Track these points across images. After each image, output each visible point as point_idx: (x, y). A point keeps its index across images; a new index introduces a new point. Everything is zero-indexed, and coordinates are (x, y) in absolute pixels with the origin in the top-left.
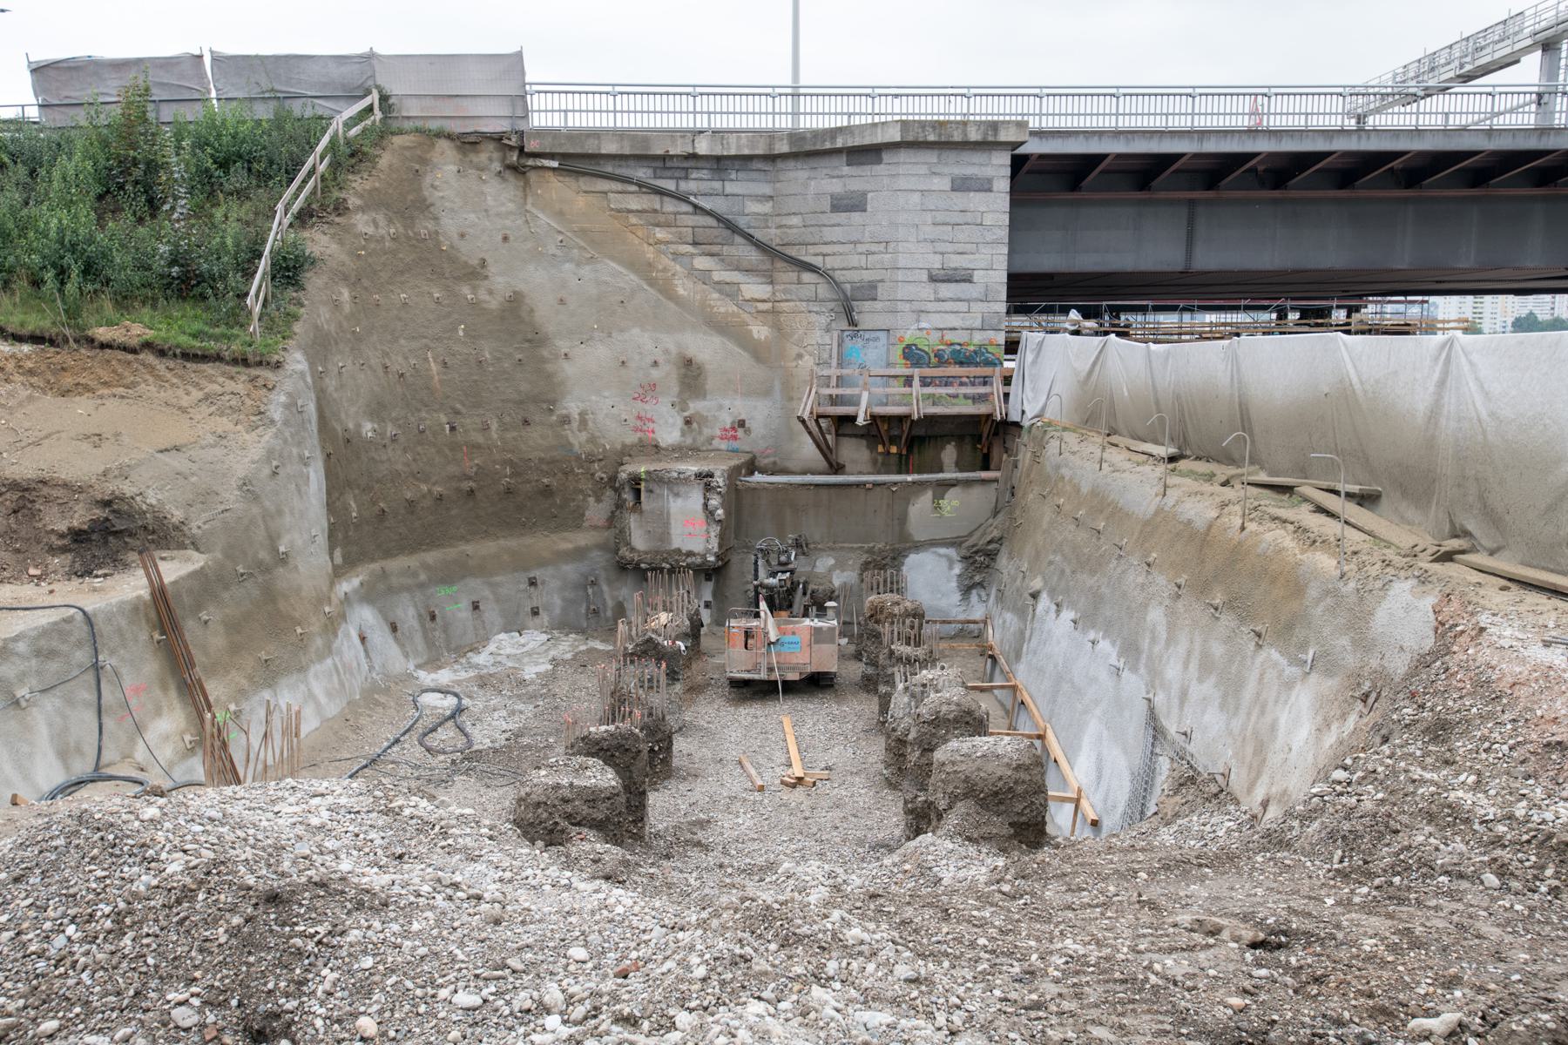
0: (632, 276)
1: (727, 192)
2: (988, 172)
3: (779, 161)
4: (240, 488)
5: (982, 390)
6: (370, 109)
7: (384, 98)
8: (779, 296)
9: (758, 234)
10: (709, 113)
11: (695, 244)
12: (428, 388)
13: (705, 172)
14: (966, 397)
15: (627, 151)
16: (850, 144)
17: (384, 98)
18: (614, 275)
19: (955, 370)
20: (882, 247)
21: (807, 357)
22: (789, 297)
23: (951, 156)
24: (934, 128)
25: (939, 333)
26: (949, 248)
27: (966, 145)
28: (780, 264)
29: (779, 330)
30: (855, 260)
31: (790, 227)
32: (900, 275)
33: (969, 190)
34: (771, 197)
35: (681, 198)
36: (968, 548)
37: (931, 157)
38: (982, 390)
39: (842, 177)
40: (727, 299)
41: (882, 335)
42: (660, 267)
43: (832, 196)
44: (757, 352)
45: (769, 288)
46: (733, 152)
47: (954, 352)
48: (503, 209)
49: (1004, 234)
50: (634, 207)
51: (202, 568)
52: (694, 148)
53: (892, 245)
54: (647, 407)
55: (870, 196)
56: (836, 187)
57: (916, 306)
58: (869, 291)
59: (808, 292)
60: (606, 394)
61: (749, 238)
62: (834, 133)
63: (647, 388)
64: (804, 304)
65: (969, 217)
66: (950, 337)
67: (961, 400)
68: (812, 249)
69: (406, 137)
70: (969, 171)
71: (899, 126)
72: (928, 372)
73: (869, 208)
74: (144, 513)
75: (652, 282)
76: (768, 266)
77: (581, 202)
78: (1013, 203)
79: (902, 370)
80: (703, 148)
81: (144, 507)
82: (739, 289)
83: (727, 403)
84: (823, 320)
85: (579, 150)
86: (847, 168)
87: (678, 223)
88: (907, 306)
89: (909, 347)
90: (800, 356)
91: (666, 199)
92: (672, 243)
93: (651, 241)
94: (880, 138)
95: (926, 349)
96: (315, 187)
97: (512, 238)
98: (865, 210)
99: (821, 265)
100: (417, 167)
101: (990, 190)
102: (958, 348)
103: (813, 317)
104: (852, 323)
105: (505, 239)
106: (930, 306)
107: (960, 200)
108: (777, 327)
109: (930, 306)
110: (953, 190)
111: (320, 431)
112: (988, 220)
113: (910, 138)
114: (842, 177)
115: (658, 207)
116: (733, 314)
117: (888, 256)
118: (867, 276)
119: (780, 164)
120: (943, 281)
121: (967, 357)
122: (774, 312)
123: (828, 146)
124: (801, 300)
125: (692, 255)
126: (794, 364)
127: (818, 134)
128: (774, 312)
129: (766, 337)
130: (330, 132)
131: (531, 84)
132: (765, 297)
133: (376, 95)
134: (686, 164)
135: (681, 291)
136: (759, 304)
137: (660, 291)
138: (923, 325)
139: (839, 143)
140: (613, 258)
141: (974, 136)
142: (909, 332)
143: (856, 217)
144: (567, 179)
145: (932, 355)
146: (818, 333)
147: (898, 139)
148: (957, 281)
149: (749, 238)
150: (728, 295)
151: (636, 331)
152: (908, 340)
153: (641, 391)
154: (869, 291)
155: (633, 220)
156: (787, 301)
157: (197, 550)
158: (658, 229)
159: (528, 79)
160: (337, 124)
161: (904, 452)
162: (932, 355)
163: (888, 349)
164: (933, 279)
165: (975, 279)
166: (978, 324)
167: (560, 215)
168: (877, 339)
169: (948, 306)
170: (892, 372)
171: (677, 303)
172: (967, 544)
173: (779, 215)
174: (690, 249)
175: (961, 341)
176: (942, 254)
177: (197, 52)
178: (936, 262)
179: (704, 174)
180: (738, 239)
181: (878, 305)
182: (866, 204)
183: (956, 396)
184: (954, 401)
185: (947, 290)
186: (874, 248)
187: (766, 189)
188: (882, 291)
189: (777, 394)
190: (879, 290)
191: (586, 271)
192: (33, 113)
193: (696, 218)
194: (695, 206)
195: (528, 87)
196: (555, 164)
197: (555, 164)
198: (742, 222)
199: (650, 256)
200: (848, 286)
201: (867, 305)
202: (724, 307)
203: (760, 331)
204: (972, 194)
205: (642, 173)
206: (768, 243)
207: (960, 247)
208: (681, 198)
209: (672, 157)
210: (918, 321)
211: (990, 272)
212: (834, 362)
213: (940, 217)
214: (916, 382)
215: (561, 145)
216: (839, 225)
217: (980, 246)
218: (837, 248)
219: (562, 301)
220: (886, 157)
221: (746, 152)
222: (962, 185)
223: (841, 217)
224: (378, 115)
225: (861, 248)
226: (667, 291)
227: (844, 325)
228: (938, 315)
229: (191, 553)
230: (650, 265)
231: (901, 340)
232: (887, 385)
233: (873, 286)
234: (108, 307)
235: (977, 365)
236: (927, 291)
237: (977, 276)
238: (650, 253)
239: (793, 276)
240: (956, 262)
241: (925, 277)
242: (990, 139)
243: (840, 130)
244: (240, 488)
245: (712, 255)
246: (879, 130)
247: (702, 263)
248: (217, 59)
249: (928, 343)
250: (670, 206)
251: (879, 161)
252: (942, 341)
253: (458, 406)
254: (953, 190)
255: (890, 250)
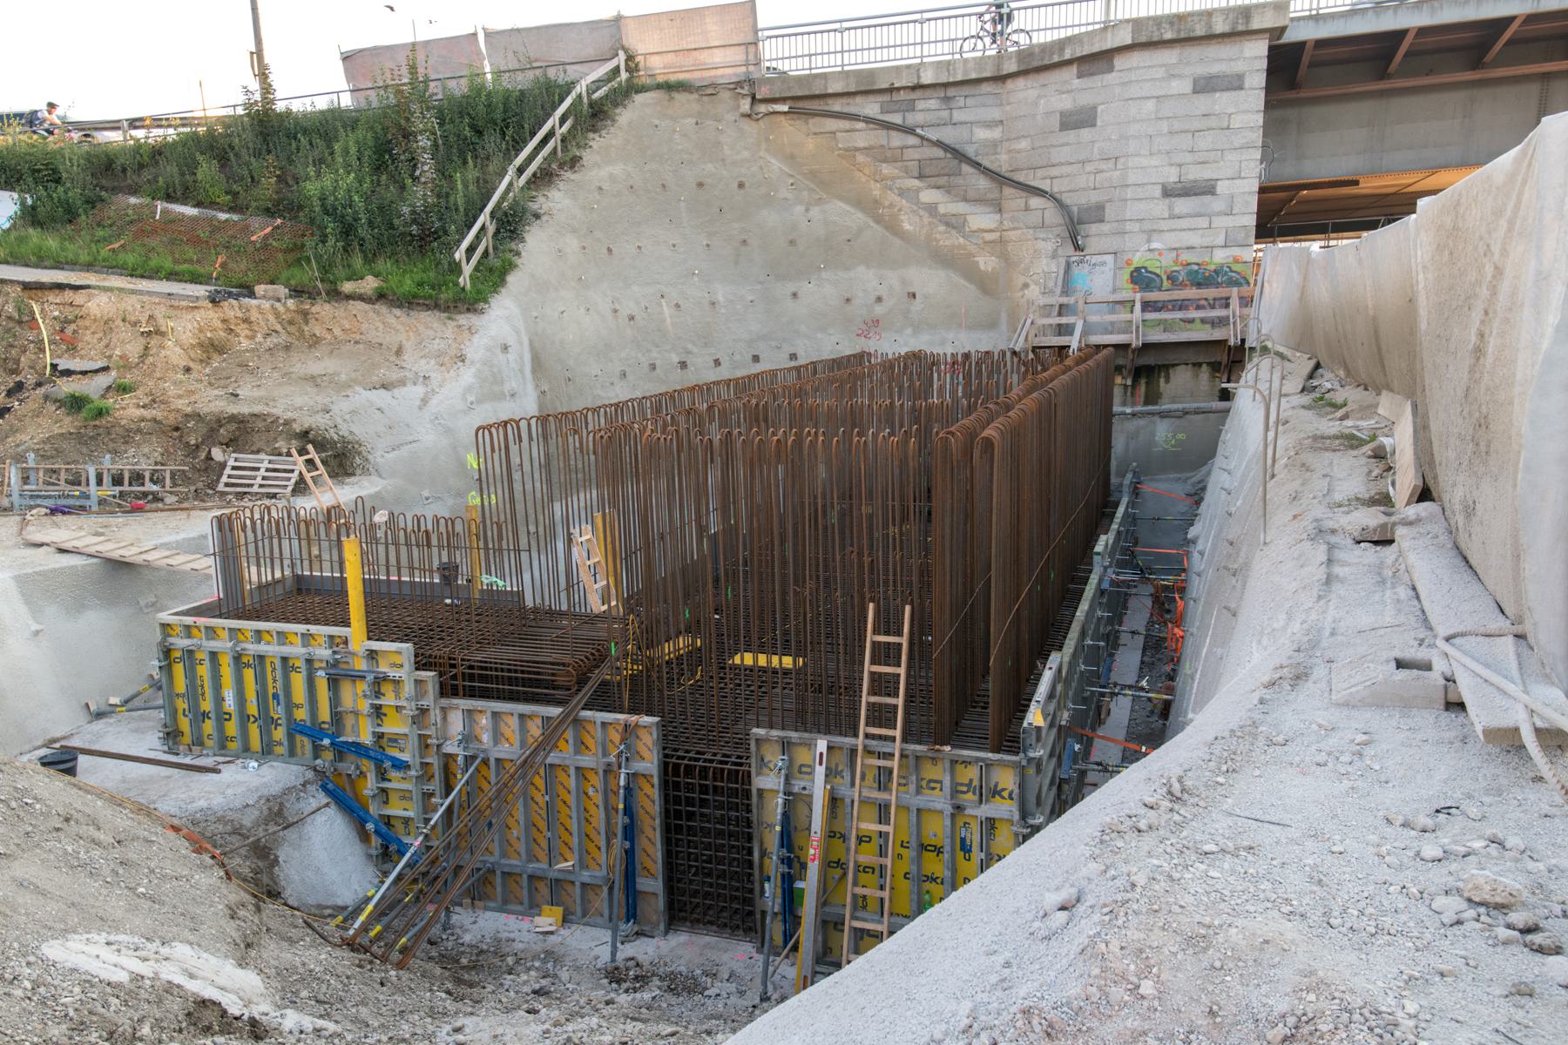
0: (860, 215)
1: (954, 121)
2: (1239, 67)
3: (1009, 81)
4: (431, 421)
5: (1218, 313)
6: (616, 71)
7: (630, 58)
8: (1007, 224)
9: (986, 162)
10: (810, 55)
11: (921, 177)
12: (659, 330)
13: (932, 101)
14: (1203, 321)
15: (852, 89)
16: (1078, 54)
17: (630, 58)
18: (841, 214)
19: (1191, 293)
20: (1111, 164)
21: (1032, 287)
22: (1016, 225)
23: (1194, 52)
24: (1172, 24)
25: (1174, 254)
26: (1189, 158)
27: (1211, 38)
28: (1008, 191)
29: (1006, 260)
30: (1082, 181)
31: (1019, 152)
32: (1129, 193)
33: (1214, 90)
34: (1002, 122)
35: (910, 131)
36: (1193, 485)
37: (1169, 56)
38: (1218, 313)
39: (1072, 91)
40: (954, 232)
41: (1109, 259)
42: (887, 203)
43: (1062, 114)
44: (985, 285)
45: (998, 217)
46: (959, 78)
47: (1190, 273)
48: (739, 157)
49: (1257, 137)
50: (861, 144)
51: (379, 492)
52: (919, 77)
53: (1122, 160)
54: (871, 343)
55: (1100, 109)
56: (1066, 103)
57: (1148, 226)
58: (1097, 213)
59: (1034, 218)
60: (831, 331)
61: (977, 165)
62: (1061, 44)
63: (870, 324)
64: (1031, 231)
65: (1213, 122)
66: (1187, 257)
67: (1198, 325)
68: (1040, 173)
69: (648, 95)
70: (1216, 69)
71: (1130, 27)
72: (1153, 296)
73: (1099, 123)
74: (335, 443)
75: (878, 220)
76: (996, 195)
77: (811, 144)
78: (1269, 105)
79: (1126, 295)
80: (927, 78)
81: (336, 438)
82: (965, 220)
83: (951, 336)
84: (1049, 246)
85: (807, 93)
86: (1077, 81)
87: (905, 158)
88: (1137, 227)
89: (1137, 270)
90: (1026, 286)
91: (893, 133)
92: (899, 178)
93: (877, 178)
94: (1109, 44)
95: (1158, 271)
96: (555, 148)
97: (747, 185)
98: (1094, 125)
99: (1048, 189)
100: (657, 122)
101: (1241, 88)
102: (1196, 267)
103: (1041, 244)
104: (1077, 248)
105: (741, 185)
106: (1163, 225)
107: (1203, 103)
108: (1004, 257)
109: (1163, 225)
110: (1195, 92)
111: (534, 371)
112: (1236, 122)
113: (1143, 39)
114: (1072, 91)
115: (884, 142)
116: (960, 247)
117: (1118, 173)
118: (1094, 198)
119: (1010, 84)
120: (1180, 195)
121: (1206, 278)
122: (1001, 241)
123: (1056, 59)
124: (1028, 228)
125: (918, 190)
126: (1020, 294)
127: (1046, 48)
128: (1001, 241)
129: (994, 269)
130: (573, 95)
131: (762, 30)
132: (993, 226)
133: (622, 56)
134: (913, 96)
135: (907, 226)
136: (985, 234)
137: (887, 228)
138: (1155, 245)
139: (1067, 55)
140: (841, 198)
141: (1220, 26)
142: (1138, 254)
143: (1085, 133)
144: (798, 122)
145: (1164, 277)
146: (1044, 261)
147: (1129, 41)
148: (1195, 194)
149: (977, 165)
150: (954, 228)
151: (861, 269)
152: (1137, 262)
153: (864, 327)
154: (1097, 213)
155: (860, 158)
156: (1014, 229)
157: (380, 476)
158: (884, 165)
159: (760, 25)
160: (581, 88)
161: (1129, 382)
162: (1164, 277)
163: (1115, 274)
164: (1168, 192)
165: (1219, 190)
166: (1220, 240)
167: (790, 158)
168: (1103, 264)
169: (1184, 223)
170: (1117, 297)
171: (902, 238)
172: (1193, 480)
173: (1008, 140)
174: (916, 183)
175: (1200, 261)
176: (1180, 166)
177: (472, 31)
178: (1172, 176)
179: (932, 104)
180: (966, 168)
181: (1105, 227)
182: (1095, 118)
183: (1191, 321)
184: (1189, 326)
185: (1183, 205)
186: (1103, 166)
187: (995, 114)
188: (1110, 212)
189: (1004, 327)
190: (1107, 210)
191: (815, 212)
192: (346, 101)
193: (926, 149)
194: (922, 138)
195: (760, 34)
196: (785, 108)
197: (785, 108)
198: (970, 151)
199: (876, 193)
200: (1075, 209)
201: (1094, 228)
202: (949, 240)
203: (986, 263)
204: (1218, 95)
205: (871, 108)
206: (998, 170)
207: (1201, 157)
208: (910, 131)
209: (899, 89)
210: (1149, 241)
211: (1237, 181)
212: (1058, 290)
213: (1177, 126)
214: (1138, 306)
215: (789, 88)
216: (1067, 144)
217: (1226, 153)
218: (1065, 170)
219: (792, 242)
220: (1119, 62)
221: (974, 76)
222: (1205, 86)
223: (1071, 136)
224: (624, 75)
225: (1089, 168)
226: (893, 227)
227: (1070, 250)
228: (1172, 234)
229: (374, 478)
230: (876, 202)
231: (1129, 263)
232: (1112, 312)
233: (1100, 208)
234: (358, 261)
235: (1218, 285)
236: (1161, 208)
237: (1221, 188)
238: (876, 190)
239: (1021, 202)
240: (1195, 174)
241: (1158, 192)
242: (1241, 28)
243: (1069, 40)
244: (431, 421)
245: (938, 188)
246: (1109, 35)
247: (929, 196)
248: (489, 35)
249: (1161, 264)
250: (897, 139)
251: (1111, 69)
252: (1176, 261)
253: (690, 346)
254: (1195, 92)
255: (1119, 166)
